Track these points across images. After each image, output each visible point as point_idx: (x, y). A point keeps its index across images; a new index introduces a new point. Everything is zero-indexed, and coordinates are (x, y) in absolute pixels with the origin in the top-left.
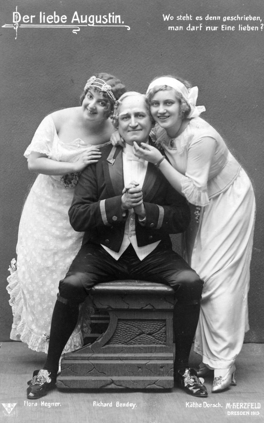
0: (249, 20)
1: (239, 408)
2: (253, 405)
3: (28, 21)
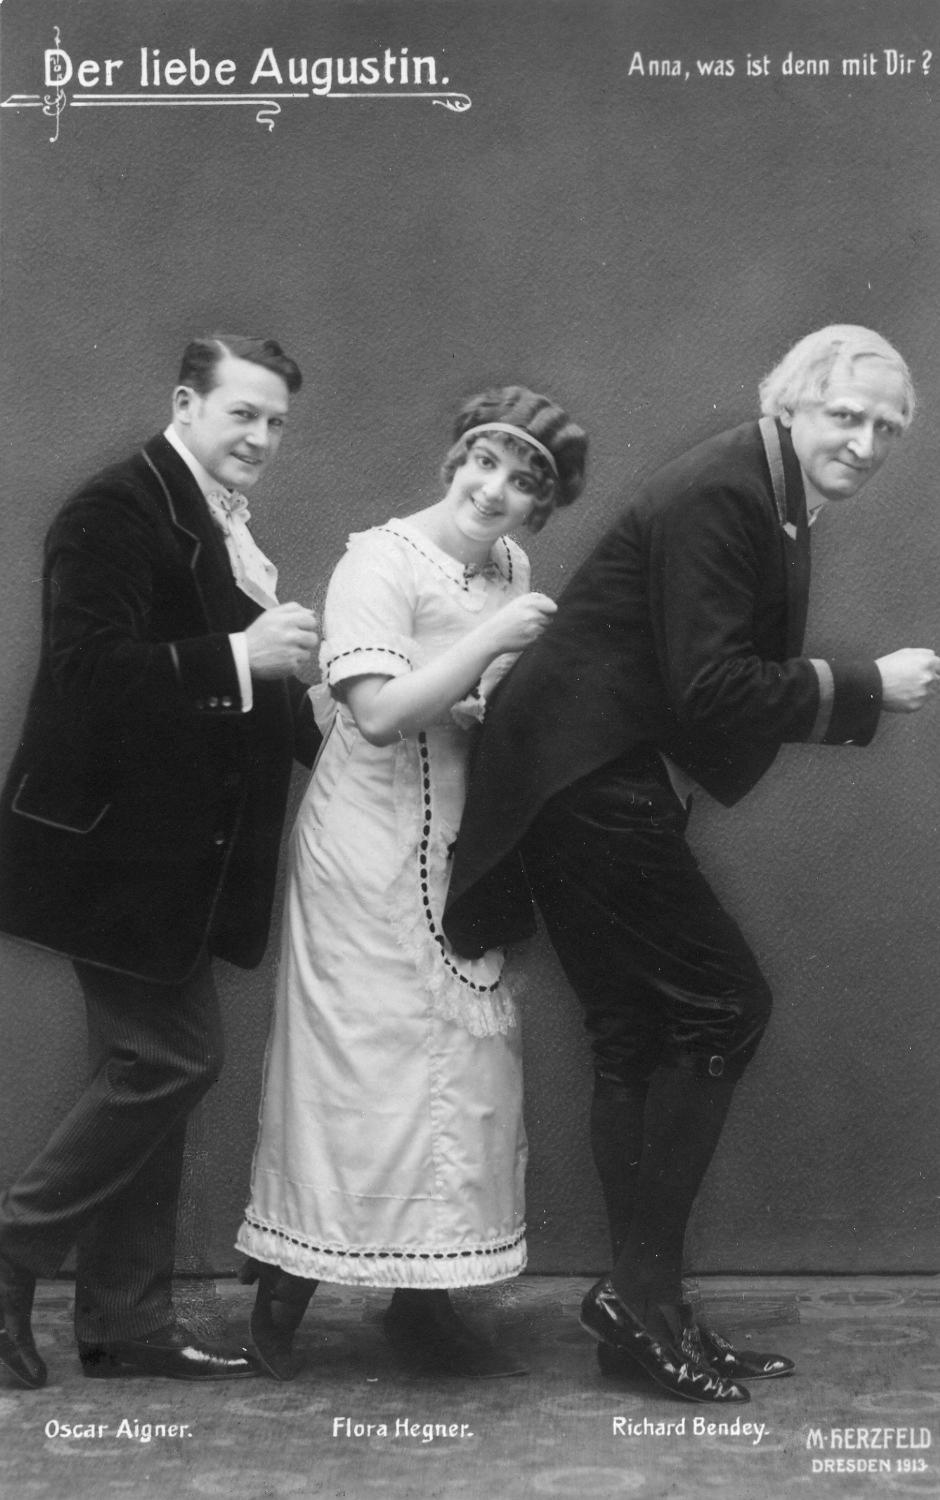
0: (671, 61)
1: (852, 1447)
2: (851, 1437)
3: (96, 81)
